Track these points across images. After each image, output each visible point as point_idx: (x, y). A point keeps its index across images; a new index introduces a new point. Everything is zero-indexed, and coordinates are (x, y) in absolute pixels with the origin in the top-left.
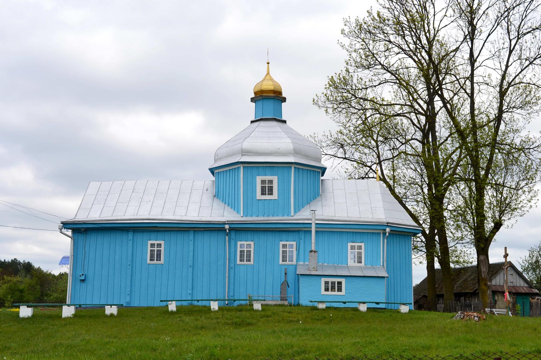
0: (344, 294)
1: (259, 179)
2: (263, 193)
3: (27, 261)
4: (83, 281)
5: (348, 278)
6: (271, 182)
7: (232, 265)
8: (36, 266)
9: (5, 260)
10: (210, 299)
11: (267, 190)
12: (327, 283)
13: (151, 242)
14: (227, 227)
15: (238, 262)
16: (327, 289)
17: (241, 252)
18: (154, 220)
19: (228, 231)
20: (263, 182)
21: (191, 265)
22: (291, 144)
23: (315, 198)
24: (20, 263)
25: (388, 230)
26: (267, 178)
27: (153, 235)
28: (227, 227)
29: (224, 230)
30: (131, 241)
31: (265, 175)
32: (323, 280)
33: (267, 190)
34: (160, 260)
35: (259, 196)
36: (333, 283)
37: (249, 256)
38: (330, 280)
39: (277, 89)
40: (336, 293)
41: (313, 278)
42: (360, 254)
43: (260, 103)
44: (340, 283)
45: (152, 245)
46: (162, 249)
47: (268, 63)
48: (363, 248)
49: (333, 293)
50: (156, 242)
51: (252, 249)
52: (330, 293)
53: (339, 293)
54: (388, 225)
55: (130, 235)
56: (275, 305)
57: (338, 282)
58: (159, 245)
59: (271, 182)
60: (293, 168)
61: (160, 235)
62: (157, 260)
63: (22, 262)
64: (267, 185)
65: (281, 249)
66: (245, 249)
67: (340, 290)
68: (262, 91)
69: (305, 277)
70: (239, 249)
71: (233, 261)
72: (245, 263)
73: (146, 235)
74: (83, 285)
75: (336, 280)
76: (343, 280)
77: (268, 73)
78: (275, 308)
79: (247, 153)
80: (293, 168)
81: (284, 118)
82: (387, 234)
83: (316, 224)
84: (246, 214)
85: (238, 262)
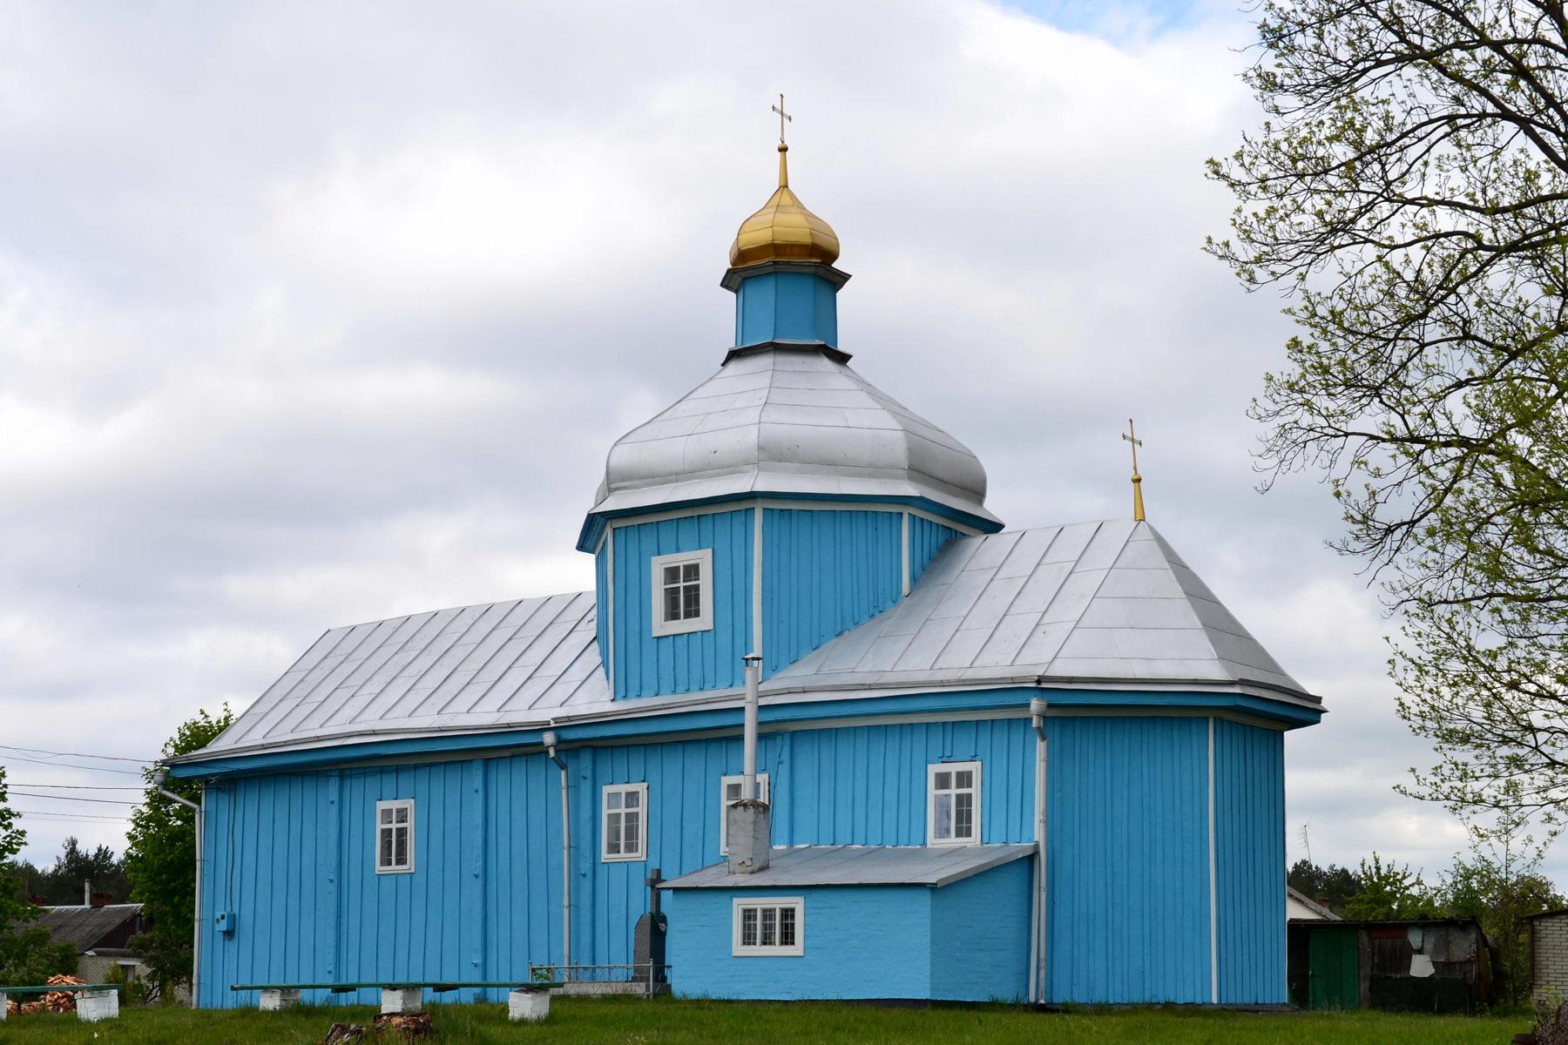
0: (800, 953)
1: (658, 566)
2: (672, 615)
3: (1338, 868)
4: (229, 934)
5: (816, 895)
6: (692, 571)
7: (586, 866)
9: (1332, 867)
10: (318, 983)
11: (683, 602)
12: (749, 915)
13: (389, 805)
14: (549, 738)
15: (605, 856)
17: (387, 833)
18: (374, 733)
19: (552, 753)
20: (672, 574)
21: (479, 871)
22: (901, 434)
23: (876, 611)
24: (1319, 875)
25: (1036, 705)
26: (681, 559)
27: (389, 782)
28: (549, 738)
29: (539, 750)
31: (678, 550)
32: (739, 904)
33: (683, 602)
34: (404, 862)
35: (660, 625)
37: (631, 833)
38: (759, 903)
39: (823, 241)
40: (777, 950)
41: (866, 903)
42: (964, 802)
43: (764, 294)
44: (788, 914)
47: (783, 150)
48: (976, 779)
50: (953, 768)
51: (642, 810)
52: (758, 950)
53: (787, 950)
54: (1042, 686)
55: (332, 789)
56: (605, 999)
57: (764, 911)
59: (692, 571)
60: (758, 517)
61: (406, 780)
62: (398, 863)
63: (1325, 869)
64: (682, 585)
65: (932, 792)
67: (788, 938)
68: (775, 248)
69: (847, 894)
70: (605, 812)
71: (588, 854)
72: (623, 855)
73: (372, 783)
74: (232, 946)
75: (778, 903)
76: (797, 903)
77: (785, 186)
79: (622, 480)
80: (758, 517)
81: (842, 347)
82: (552, 753)
83: (761, 708)
84: (622, 690)
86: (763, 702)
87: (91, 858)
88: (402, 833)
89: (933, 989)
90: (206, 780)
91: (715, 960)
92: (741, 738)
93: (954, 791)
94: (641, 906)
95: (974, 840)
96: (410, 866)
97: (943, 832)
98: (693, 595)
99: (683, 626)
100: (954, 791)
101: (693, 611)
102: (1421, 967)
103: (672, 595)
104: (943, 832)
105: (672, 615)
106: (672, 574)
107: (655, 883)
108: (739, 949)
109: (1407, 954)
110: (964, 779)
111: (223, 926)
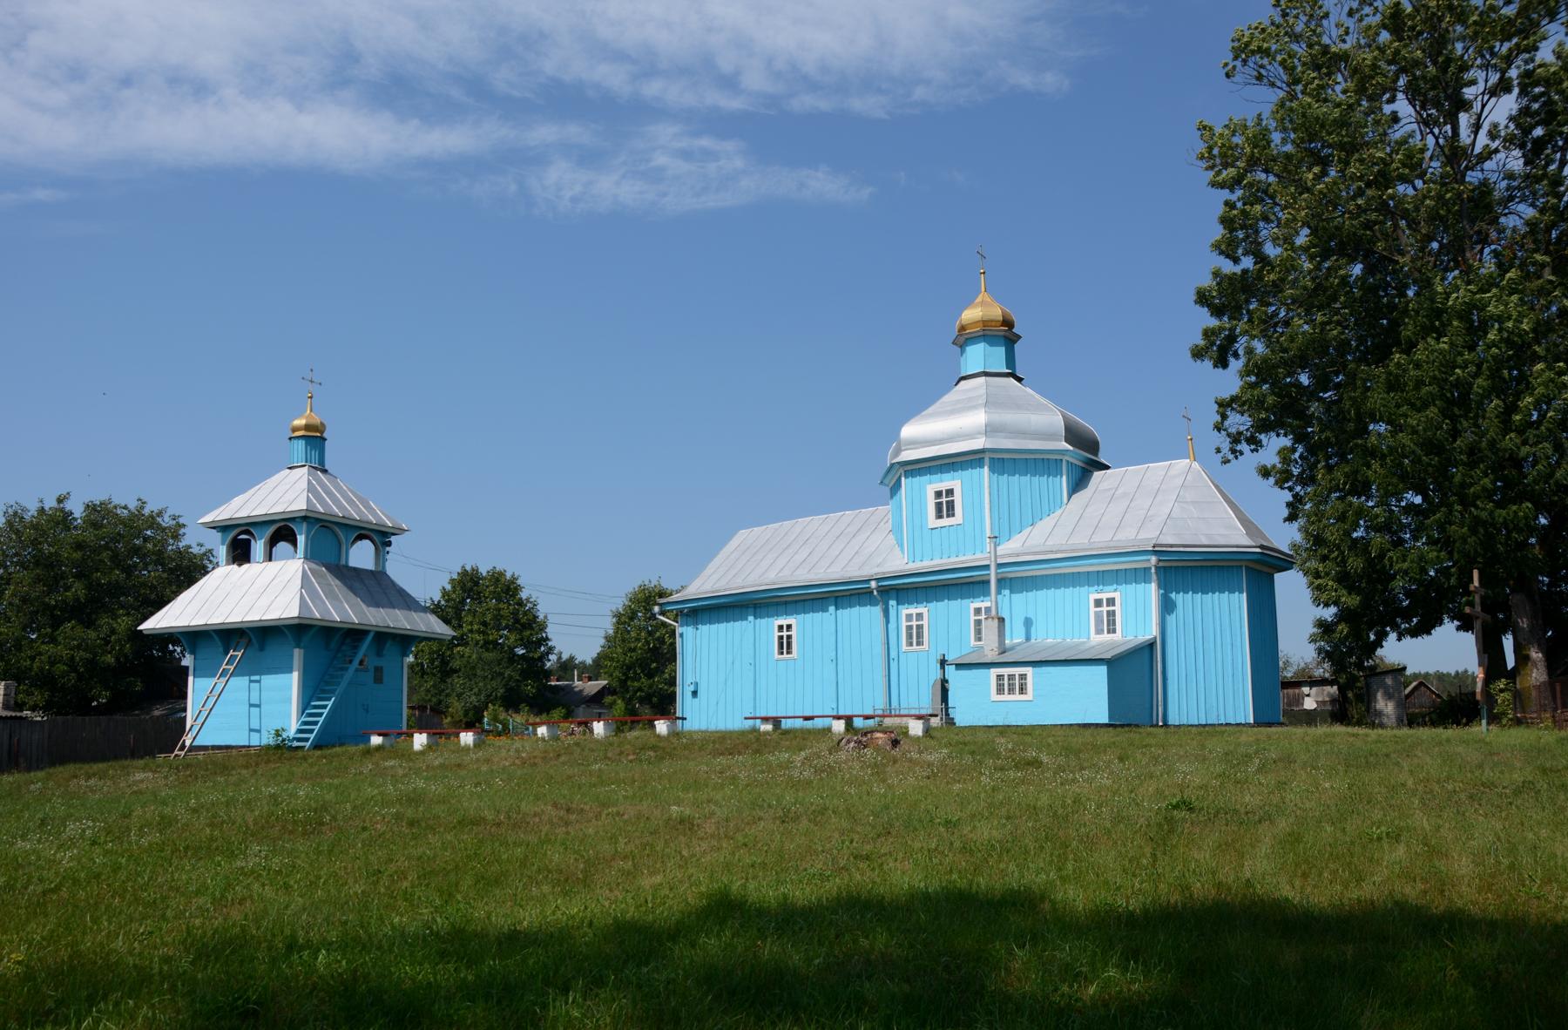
6: (950, 492)
8: (1431, 671)
11: (945, 508)
12: (1000, 677)
14: (873, 584)
15: (904, 647)
16: (1000, 690)
17: (909, 628)
20: (938, 494)
28: (873, 584)
30: (1016, 605)
32: (994, 672)
35: (932, 521)
36: (1011, 677)
38: (1006, 671)
40: (1017, 697)
42: (1111, 614)
44: (1023, 677)
45: (909, 617)
46: (1117, 608)
49: (1011, 697)
50: (1104, 596)
52: (1006, 697)
58: (920, 616)
59: (950, 492)
66: (914, 623)
67: (1022, 690)
76: (1028, 671)
78: (1061, 732)
80: (987, 460)
85: (904, 647)
86: (1000, 561)
87: (551, 662)
88: (920, 627)
89: (1110, 718)
90: (681, 611)
91: (979, 703)
92: (988, 582)
93: (1105, 609)
94: (936, 674)
95: (1118, 636)
96: (925, 646)
97: (1099, 631)
98: (951, 505)
99: (945, 521)
100: (1105, 609)
101: (951, 513)
102: (1310, 704)
103: (939, 506)
104: (1099, 631)
105: (939, 516)
106: (938, 494)
107: (943, 663)
108: (995, 697)
109: (1302, 697)
110: (1111, 602)
111: (692, 688)
